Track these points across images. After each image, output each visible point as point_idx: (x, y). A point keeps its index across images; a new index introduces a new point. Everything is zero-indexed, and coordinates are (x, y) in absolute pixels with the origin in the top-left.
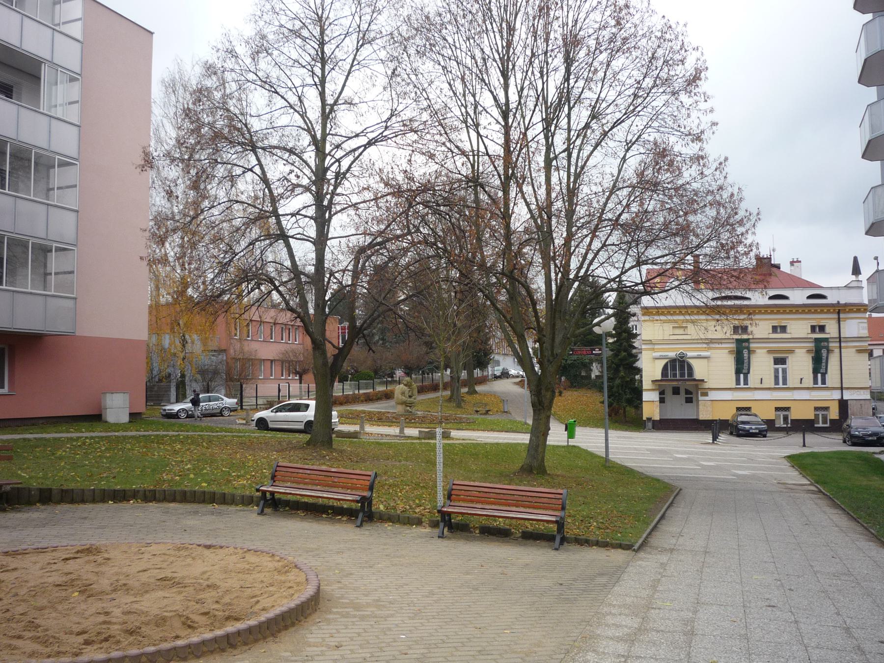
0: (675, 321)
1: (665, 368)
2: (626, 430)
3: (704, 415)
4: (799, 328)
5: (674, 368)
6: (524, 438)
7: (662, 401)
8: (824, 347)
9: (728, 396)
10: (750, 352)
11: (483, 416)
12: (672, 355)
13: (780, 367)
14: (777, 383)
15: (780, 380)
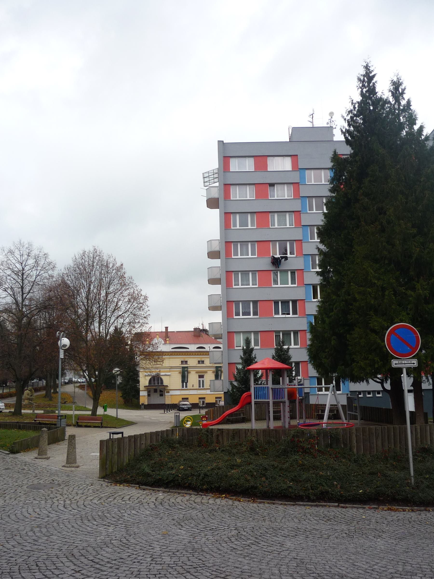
1: (150, 381)
2: (132, 409)
3: (168, 401)
5: (154, 380)
6: (90, 413)
7: (149, 395)
8: (220, 370)
9: (178, 393)
10: (188, 372)
11: (63, 405)
12: (154, 374)
13: (201, 379)
14: (200, 387)
15: (201, 385)
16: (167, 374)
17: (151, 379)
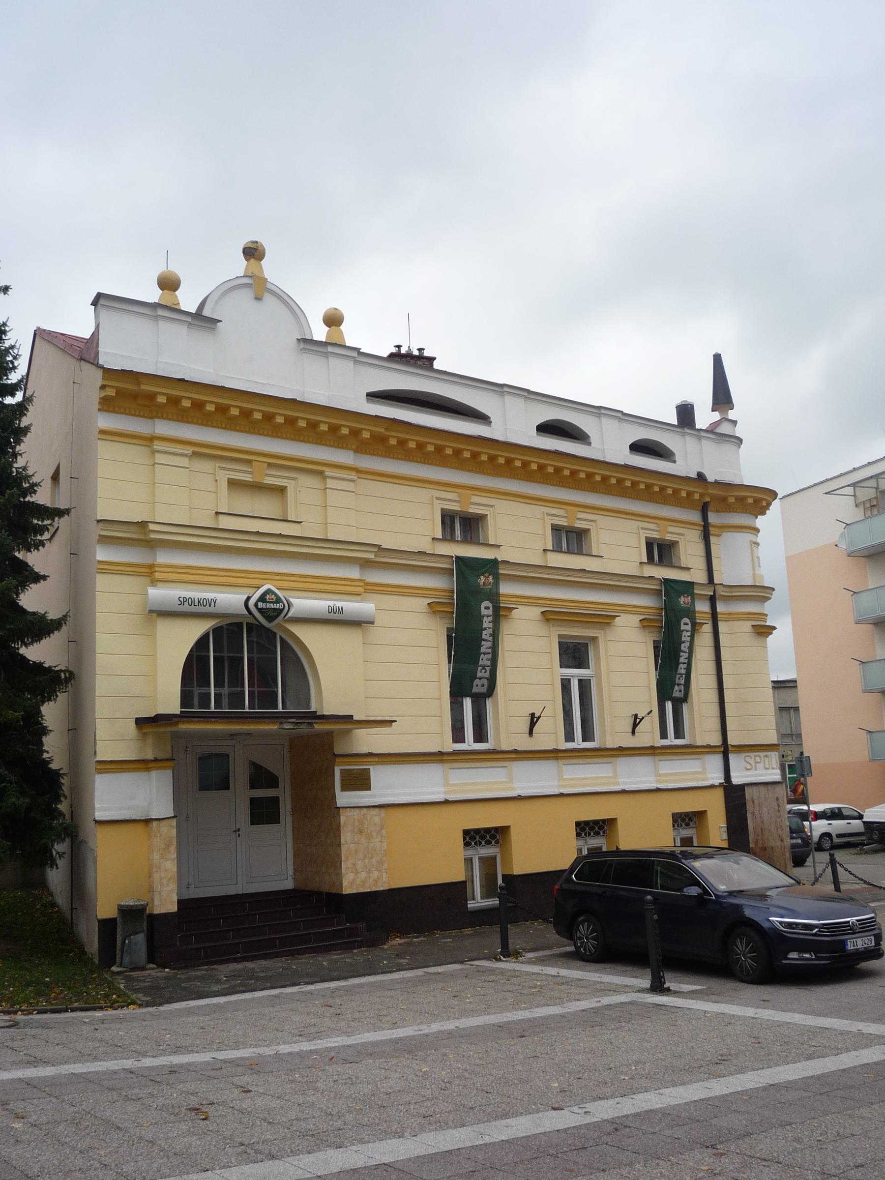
0: (245, 458)
1: (194, 668)
4: (618, 544)
5: (230, 670)
10: (499, 613)
12: (230, 600)
16: (351, 606)
17: (202, 643)
